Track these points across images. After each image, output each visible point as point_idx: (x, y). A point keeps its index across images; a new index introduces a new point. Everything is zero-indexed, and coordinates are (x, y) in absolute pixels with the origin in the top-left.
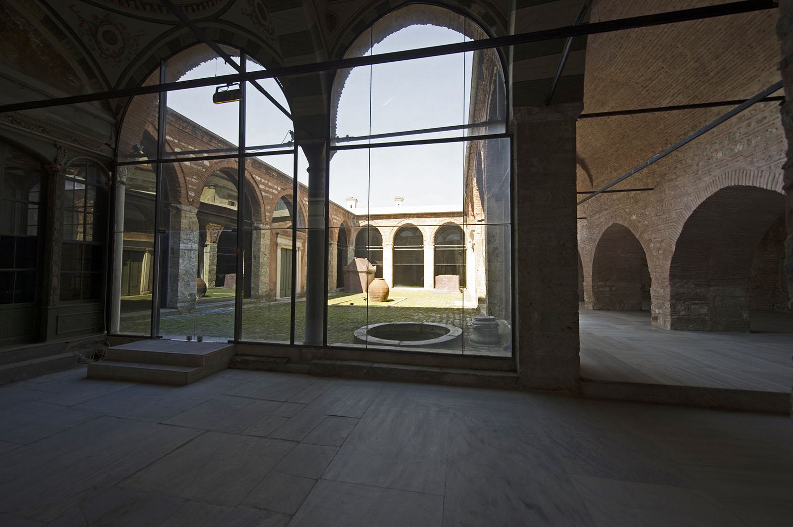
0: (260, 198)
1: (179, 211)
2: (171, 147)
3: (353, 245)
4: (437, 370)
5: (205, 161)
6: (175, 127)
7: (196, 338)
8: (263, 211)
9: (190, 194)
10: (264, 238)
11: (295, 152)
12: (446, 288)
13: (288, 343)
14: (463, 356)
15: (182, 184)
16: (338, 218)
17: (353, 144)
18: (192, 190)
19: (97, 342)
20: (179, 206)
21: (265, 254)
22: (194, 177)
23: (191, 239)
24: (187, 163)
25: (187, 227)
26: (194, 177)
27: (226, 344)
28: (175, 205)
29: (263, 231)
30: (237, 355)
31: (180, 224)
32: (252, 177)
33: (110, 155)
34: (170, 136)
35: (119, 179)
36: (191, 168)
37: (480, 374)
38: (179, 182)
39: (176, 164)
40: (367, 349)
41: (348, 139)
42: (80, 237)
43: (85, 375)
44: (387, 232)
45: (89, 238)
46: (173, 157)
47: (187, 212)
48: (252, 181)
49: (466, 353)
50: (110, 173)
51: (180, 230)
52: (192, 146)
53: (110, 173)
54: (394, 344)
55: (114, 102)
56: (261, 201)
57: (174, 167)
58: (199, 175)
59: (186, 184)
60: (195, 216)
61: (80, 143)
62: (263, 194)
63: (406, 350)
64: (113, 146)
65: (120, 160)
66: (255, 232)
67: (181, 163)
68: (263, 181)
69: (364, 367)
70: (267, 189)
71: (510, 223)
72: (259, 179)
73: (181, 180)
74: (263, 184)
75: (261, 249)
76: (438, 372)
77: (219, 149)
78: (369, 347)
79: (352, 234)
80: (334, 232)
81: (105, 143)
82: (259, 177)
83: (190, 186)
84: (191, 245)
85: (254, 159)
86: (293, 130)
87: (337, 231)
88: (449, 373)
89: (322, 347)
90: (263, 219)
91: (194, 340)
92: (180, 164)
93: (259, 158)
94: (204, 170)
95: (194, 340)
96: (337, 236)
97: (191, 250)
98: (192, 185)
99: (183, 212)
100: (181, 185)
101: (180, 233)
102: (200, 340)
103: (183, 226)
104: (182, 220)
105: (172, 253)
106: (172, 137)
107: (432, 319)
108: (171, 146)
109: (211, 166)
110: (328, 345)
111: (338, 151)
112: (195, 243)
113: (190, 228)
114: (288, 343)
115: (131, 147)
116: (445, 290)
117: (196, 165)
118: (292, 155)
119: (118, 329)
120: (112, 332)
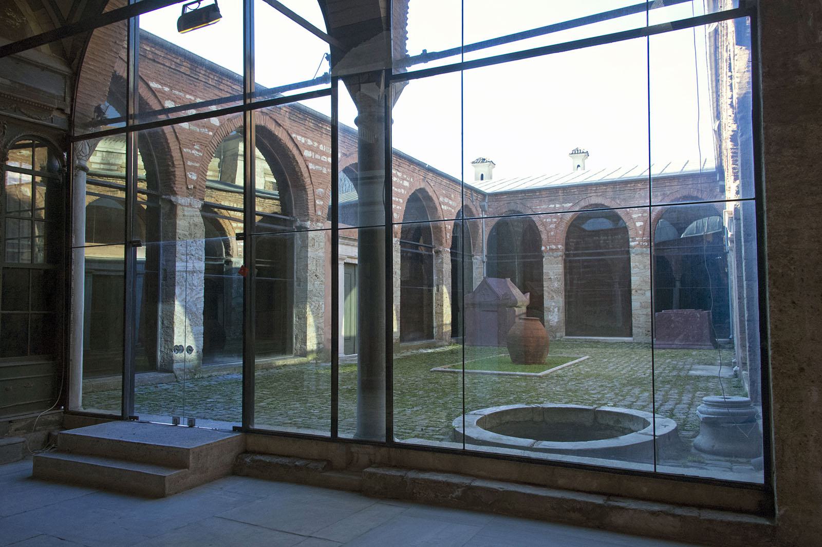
0: (306, 175)
1: (173, 207)
2: (159, 101)
3: (482, 252)
4: (599, 500)
5: (212, 119)
6: (164, 65)
7: (186, 420)
8: (310, 197)
9: (190, 176)
10: (313, 245)
11: (333, 92)
12: (681, 337)
13: (328, 434)
14: (655, 475)
15: (177, 160)
16: (451, 203)
17: (438, 64)
18: (193, 169)
19: (50, 423)
20: (173, 199)
21: (316, 276)
22: (196, 147)
23: (193, 253)
24: (185, 125)
25: (187, 233)
26: (196, 147)
27: (230, 432)
28: (167, 197)
29: (311, 234)
30: (246, 452)
31: (176, 229)
32: (291, 137)
33: (65, 127)
34: (158, 82)
35: (77, 162)
36: (192, 132)
37: (689, 514)
38: (172, 157)
39: (167, 129)
40: (464, 452)
41: (426, 56)
42: (26, 257)
43: (30, 473)
44: (551, 223)
45: (40, 257)
46: (163, 117)
47: (186, 208)
48: (290, 145)
49: (662, 469)
50: (65, 154)
51: (175, 239)
52: (190, 94)
53: (65, 154)
54: (522, 445)
55: (67, 42)
56: (307, 181)
57: (164, 134)
58: (204, 143)
59: (183, 162)
60: (199, 213)
61: (22, 112)
62: (311, 166)
63: (495, 452)
64: (68, 111)
65: (78, 132)
66: (298, 235)
67: (175, 126)
68: (310, 142)
69: (458, 486)
70: (318, 157)
71: (754, 196)
72: (303, 141)
73: (176, 154)
74: (310, 148)
75: (310, 267)
76: (600, 506)
77: (235, 96)
78: (469, 447)
79: (480, 231)
80: (443, 229)
81: (56, 107)
82: (303, 136)
83: (189, 163)
84: (193, 263)
85: (293, 106)
86: (329, 53)
87: (450, 226)
88: (622, 508)
89: (383, 443)
90: (311, 211)
91: (184, 424)
92: (173, 127)
93: (304, 103)
94: (211, 133)
95: (184, 424)
96: (449, 236)
97: (194, 272)
98: (193, 161)
99: (179, 208)
100: (175, 163)
101: (175, 245)
102: (191, 424)
103: (180, 231)
104: (178, 222)
105: (165, 279)
106: (161, 84)
107: (629, 399)
108: (159, 98)
109: (222, 125)
110: (397, 440)
111: (410, 81)
112: (199, 259)
113: (190, 234)
114: (328, 434)
115: (93, 109)
116: (676, 342)
117: (198, 126)
118: (328, 99)
119: (80, 404)
120: (72, 407)
